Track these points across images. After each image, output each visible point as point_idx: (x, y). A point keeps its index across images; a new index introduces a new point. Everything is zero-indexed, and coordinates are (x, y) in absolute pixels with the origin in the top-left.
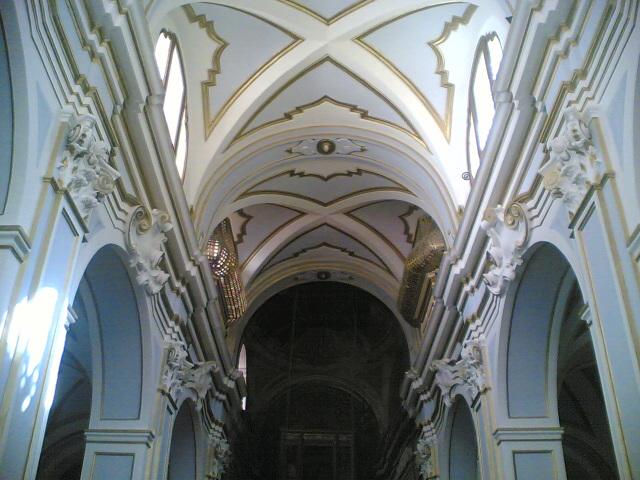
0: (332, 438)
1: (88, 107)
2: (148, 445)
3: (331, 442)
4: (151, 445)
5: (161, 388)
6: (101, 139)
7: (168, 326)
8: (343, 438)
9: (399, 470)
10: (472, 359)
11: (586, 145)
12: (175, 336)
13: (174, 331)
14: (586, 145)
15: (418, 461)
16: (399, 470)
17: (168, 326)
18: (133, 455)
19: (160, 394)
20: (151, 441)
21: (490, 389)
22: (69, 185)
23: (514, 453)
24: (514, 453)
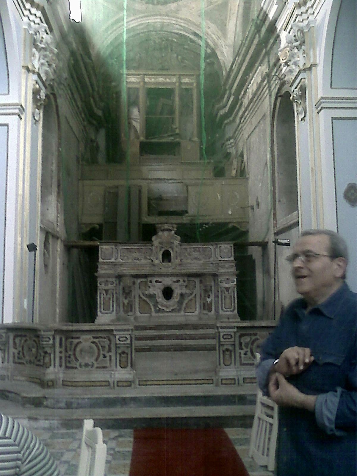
0: (174, 80)
1: (40, 18)
2: (19, 116)
3: (174, 83)
4: (23, 117)
5: (25, 65)
6: (42, 22)
7: (25, 9)
8: (186, 80)
9: (246, 101)
10: (296, 41)
11: (301, 45)
12: (37, 21)
13: (29, 10)
14: (301, 45)
15: (279, 57)
16: (246, 101)
17: (25, 9)
18: (7, 125)
19: (24, 70)
20: (22, 114)
21: (315, 65)
22: (39, 69)
23: (333, 119)
24: (333, 119)
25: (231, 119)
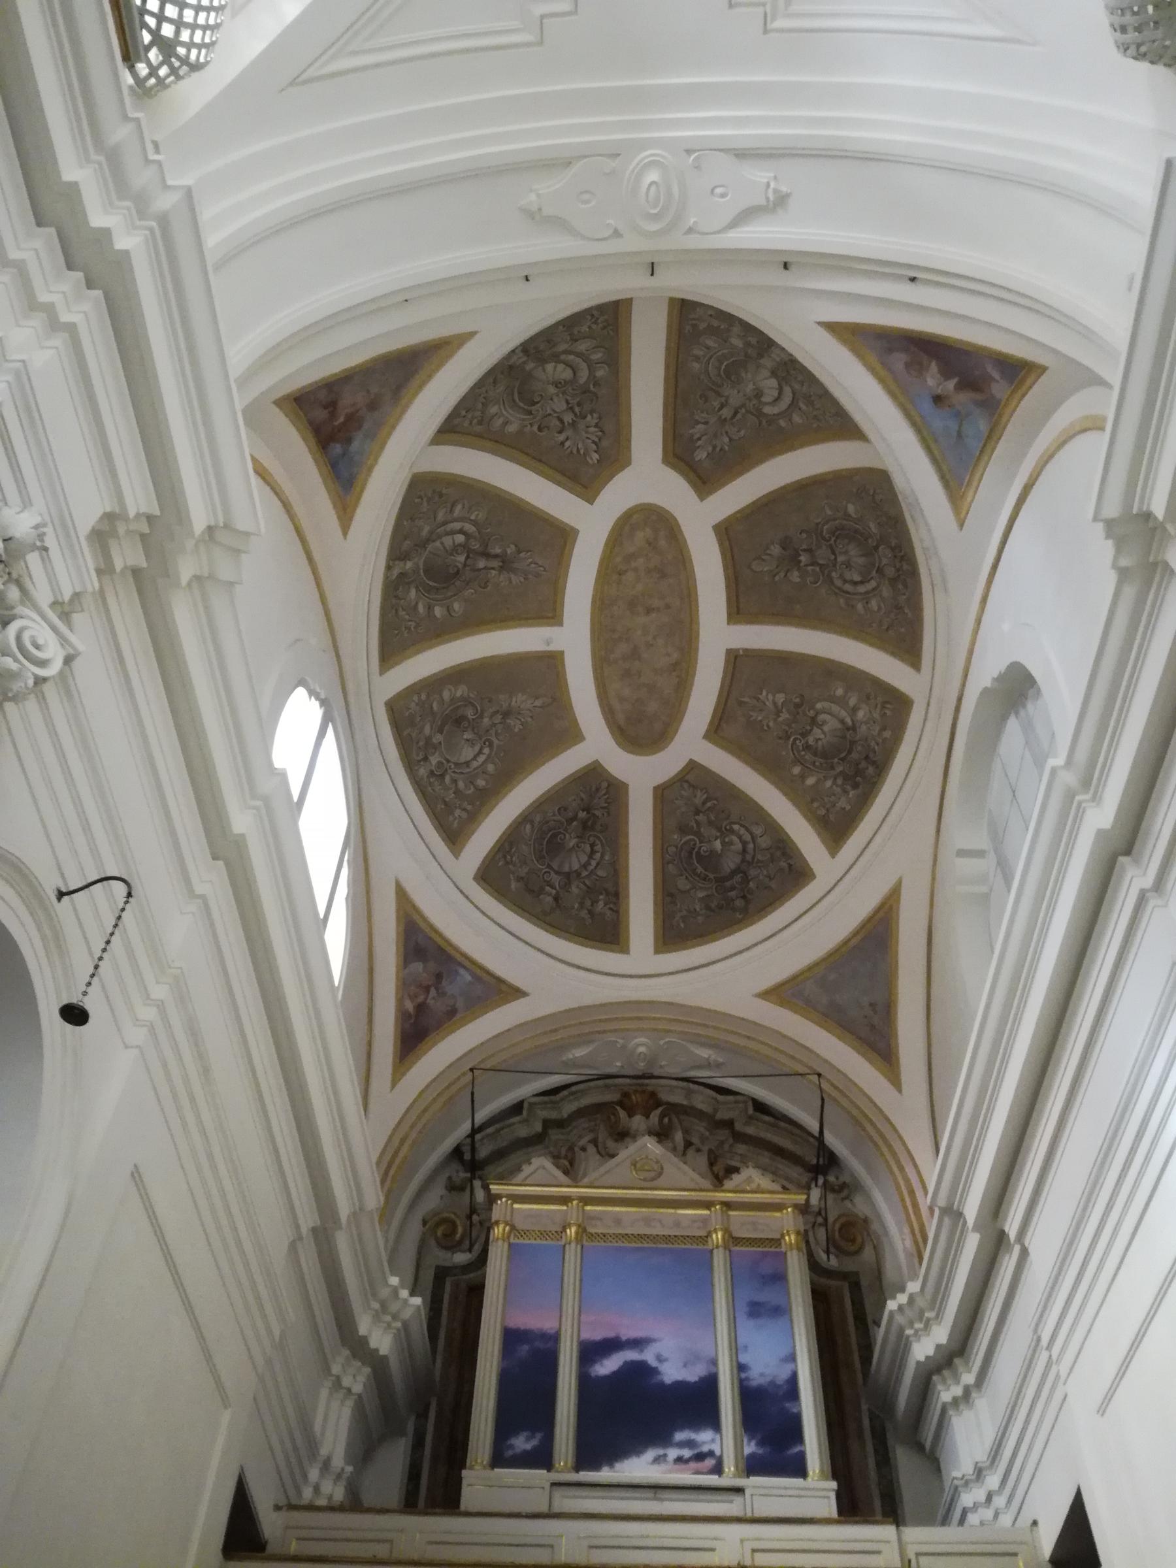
25: (969, 1378)
